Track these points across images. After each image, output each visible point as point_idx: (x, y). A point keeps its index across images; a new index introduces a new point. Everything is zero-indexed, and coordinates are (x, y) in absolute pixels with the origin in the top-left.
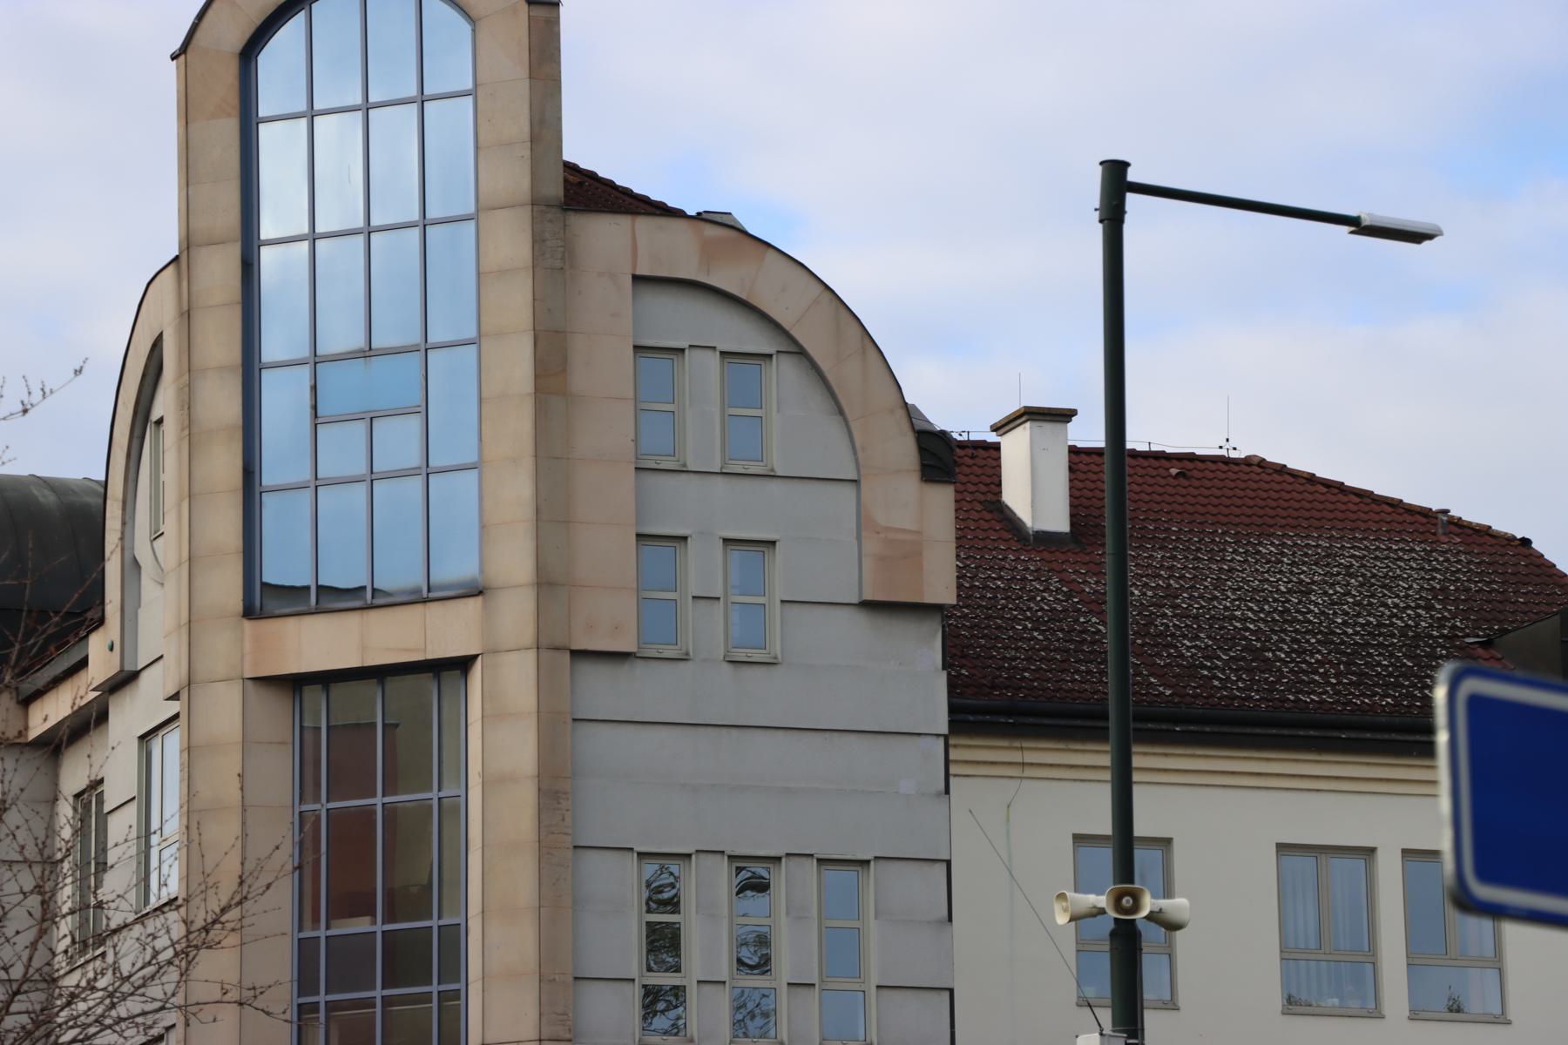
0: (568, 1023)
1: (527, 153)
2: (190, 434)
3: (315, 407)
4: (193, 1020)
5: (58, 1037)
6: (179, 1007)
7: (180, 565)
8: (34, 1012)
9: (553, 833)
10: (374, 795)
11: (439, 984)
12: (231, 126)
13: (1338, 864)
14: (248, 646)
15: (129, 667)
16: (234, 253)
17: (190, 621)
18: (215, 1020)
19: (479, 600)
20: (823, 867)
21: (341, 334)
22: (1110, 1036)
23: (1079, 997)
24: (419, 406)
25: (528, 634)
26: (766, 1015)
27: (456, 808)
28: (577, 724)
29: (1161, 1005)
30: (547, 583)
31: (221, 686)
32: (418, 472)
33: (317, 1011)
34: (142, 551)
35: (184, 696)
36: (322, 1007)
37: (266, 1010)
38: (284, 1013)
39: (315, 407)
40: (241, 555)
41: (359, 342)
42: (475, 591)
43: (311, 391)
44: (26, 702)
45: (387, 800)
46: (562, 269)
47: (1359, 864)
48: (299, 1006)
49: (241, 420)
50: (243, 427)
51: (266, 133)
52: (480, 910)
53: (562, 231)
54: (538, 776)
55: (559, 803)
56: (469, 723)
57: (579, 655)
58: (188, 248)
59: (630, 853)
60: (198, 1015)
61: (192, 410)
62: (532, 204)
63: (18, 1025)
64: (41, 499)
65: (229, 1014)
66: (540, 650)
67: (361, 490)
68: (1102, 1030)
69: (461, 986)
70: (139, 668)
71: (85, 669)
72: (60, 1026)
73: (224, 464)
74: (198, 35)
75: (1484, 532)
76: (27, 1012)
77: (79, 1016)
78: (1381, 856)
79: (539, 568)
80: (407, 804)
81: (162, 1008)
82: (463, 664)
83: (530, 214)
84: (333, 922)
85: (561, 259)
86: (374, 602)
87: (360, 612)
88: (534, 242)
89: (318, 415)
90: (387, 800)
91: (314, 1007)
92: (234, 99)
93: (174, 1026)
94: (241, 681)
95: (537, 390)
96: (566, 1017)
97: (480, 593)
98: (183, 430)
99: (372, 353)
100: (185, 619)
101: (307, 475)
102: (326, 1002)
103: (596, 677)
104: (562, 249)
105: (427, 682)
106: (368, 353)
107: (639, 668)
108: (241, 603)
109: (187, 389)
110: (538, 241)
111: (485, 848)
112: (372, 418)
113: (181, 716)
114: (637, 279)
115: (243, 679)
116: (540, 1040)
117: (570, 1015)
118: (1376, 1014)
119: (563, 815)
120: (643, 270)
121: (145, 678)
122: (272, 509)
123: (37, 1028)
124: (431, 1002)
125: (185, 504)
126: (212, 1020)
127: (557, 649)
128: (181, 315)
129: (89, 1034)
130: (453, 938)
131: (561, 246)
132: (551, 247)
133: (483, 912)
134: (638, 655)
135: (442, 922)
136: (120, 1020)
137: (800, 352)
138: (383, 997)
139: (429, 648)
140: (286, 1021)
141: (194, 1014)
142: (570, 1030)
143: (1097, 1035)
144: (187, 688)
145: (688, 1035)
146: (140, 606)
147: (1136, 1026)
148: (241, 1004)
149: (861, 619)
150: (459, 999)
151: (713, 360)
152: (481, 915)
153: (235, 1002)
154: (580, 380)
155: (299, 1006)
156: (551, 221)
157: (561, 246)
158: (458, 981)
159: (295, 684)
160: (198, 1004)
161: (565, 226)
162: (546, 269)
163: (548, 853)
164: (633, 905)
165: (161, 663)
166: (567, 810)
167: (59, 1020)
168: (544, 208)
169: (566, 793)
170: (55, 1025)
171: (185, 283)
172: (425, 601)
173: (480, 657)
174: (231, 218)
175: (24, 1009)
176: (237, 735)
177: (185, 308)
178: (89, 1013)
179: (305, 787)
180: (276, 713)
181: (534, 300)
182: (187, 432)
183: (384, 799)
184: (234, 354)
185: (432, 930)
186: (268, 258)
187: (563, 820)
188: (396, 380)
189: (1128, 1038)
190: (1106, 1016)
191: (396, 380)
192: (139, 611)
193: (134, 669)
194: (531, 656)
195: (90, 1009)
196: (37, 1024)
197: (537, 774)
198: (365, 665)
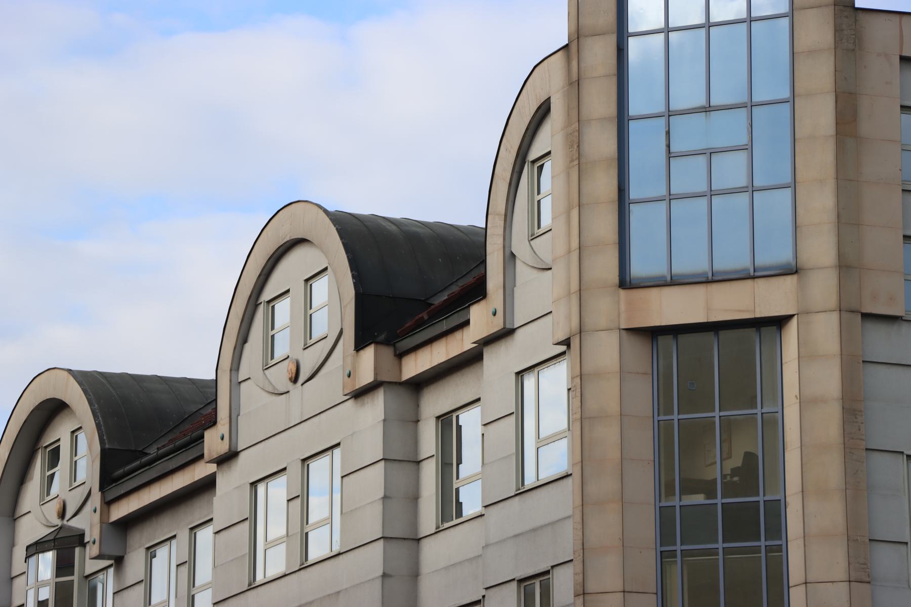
2: (579, 163)
3: (668, 146)
9: (853, 438)
14: (623, 307)
15: (508, 326)
16: (611, 41)
17: (580, 290)
19: (795, 277)
24: (747, 145)
25: (832, 300)
27: (775, 422)
31: (603, 334)
32: (746, 190)
33: (675, 556)
34: (520, 245)
35: (575, 343)
36: (679, 553)
39: (668, 146)
40: (618, 245)
41: (701, 101)
42: (792, 270)
43: (666, 135)
45: (722, 414)
46: (854, 50)
49: (617, 154)
50: (618, 159)
52: (801, 489)
53: (854, 24)
54: (842, 399)
55: (856, 418)
57: (866, 316)
58: (578, 38)
59: (901, 456)
61: (581, 147)
62: (835, 5)
64: (387, 227)
66: (841, 312)
67: (704, 202)
69: (783, 542)
70: (516, 326)
71: (468, 327)
79: (840, 255)
80: (738, 417)
82: (780, 322)
83: (833, 11)
84: (683, 497)
85: (853, 44)
86: (713, 278)
87: (705, 285)
88: (836, 30)
89: (671, 152)
90: (722, 414)
91: (673, 554)
94: (619, 330)
95: (837, 133)
96: (865, 566)
97: (796, 272)
98: (572, 161)
99: (711, 109)
100: (575, 286)
103: (877, 332)
104: (853, 36)
105: (751, 332)
106: (707, 109)
108: (618, 278)
109: (577, 134)
111: (803, 447)
112: (711, 153)
115: (620, 329)
116: (850, 581)
117: (869, 565)
119: (859, 426)
125: (575, 213)
127: (853, 312)
128: (571, 84)
130: (776, 510)
131: (853, 35)
132: (847, 35)
133: (803, 491)
134: (903, 318)
135: (766, 498)
139: (757, 309)
144: (578, 336)
146: (515, 286)
150: (781, 551)
152: (801, 493)
154: (866, 127)
156: (846, 17)
157: (853, 35)
161: (856, 20)
162: (843, 50)
163: (850, 452)
164: (904, 491)
165: (550, 316)
166: (862, 423)
168: (842, 8)
169: (861, 411)
171: (574, 63)
172: (754, 278)
173: (795, 319)
176: (616, 367)
177: (575, 77)
179: (662, 403)
181: (836, 71)
182: (576, 162)
183: (679, 416)
184: (611, 109)
185: (675, 508)
186: (634, 46)
187: (860, 430)
192: (515, 289)
193: (512, 327)
194: (835, 316)
197: (841, 397)
198: (710, 320)
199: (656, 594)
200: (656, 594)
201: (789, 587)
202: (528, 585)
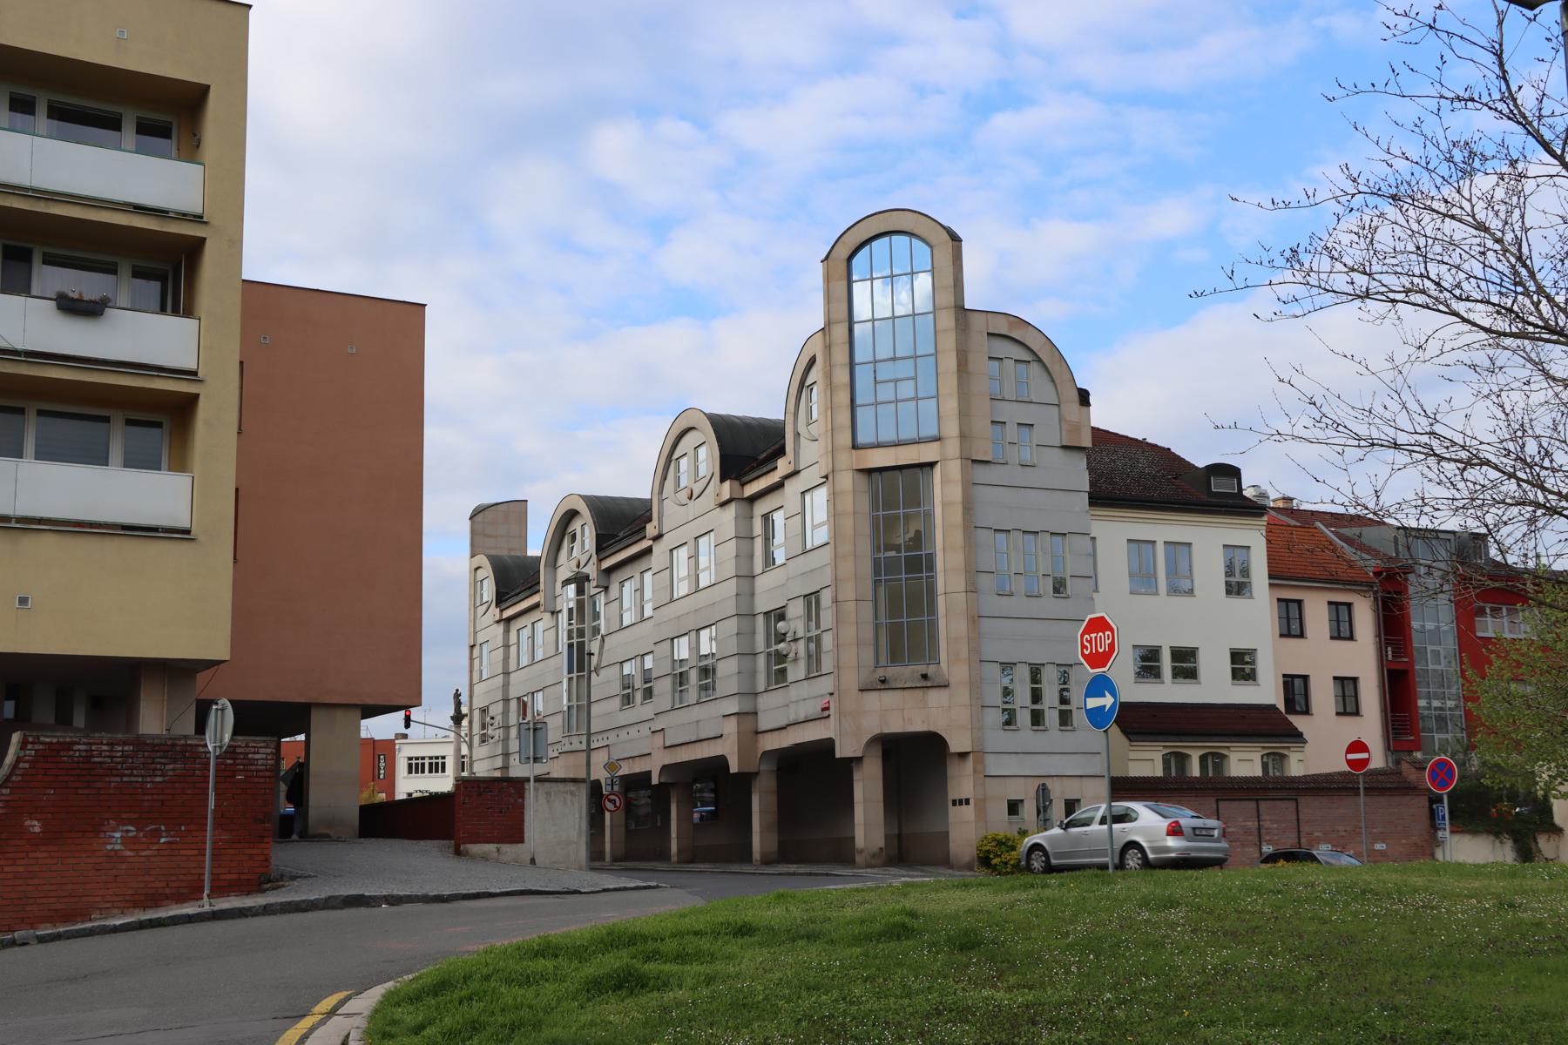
1: (953, 290)
7: (827, 431)
12: (844, 283)
13: (1144, 546)
15: (797, 469)
16: (847, 324)
19: (938, 443)
21: (884, 352)
25: (958, 454)
30: (964, 437)
42: (938, 439)
44: (743, 485)
47: (1150, 546)
51: (855, 286)
57: (974, 461)
73: (843, 397)
74: (832, 253)
75: (1156, 446)
78: (1158, 543)
82: (932, 465)
92: (845, 274)
95: (958, 370)
97: (939, 440)
100: (830, 449)
101: (874, 401)
103: (980, 469)
105: (917, 470)
106: (894, 359)
107: (992, 466)
110: (957, 320)
114: (989, 334)
118: (1157, 593)
120: (990, 331)
121: (802, 473)
122: (859, 411)
128: (826, 347)
130: (931, 558)
137: (1040, 361)
149: (1060, 452)
154: (972, 367)
159: (869, 471)
174: (844, 314)
179: (875, 505)
180: (863, 480)
184: (847, 360)
188: (905, 368)
191: (905, 368)
194: (959, 461)
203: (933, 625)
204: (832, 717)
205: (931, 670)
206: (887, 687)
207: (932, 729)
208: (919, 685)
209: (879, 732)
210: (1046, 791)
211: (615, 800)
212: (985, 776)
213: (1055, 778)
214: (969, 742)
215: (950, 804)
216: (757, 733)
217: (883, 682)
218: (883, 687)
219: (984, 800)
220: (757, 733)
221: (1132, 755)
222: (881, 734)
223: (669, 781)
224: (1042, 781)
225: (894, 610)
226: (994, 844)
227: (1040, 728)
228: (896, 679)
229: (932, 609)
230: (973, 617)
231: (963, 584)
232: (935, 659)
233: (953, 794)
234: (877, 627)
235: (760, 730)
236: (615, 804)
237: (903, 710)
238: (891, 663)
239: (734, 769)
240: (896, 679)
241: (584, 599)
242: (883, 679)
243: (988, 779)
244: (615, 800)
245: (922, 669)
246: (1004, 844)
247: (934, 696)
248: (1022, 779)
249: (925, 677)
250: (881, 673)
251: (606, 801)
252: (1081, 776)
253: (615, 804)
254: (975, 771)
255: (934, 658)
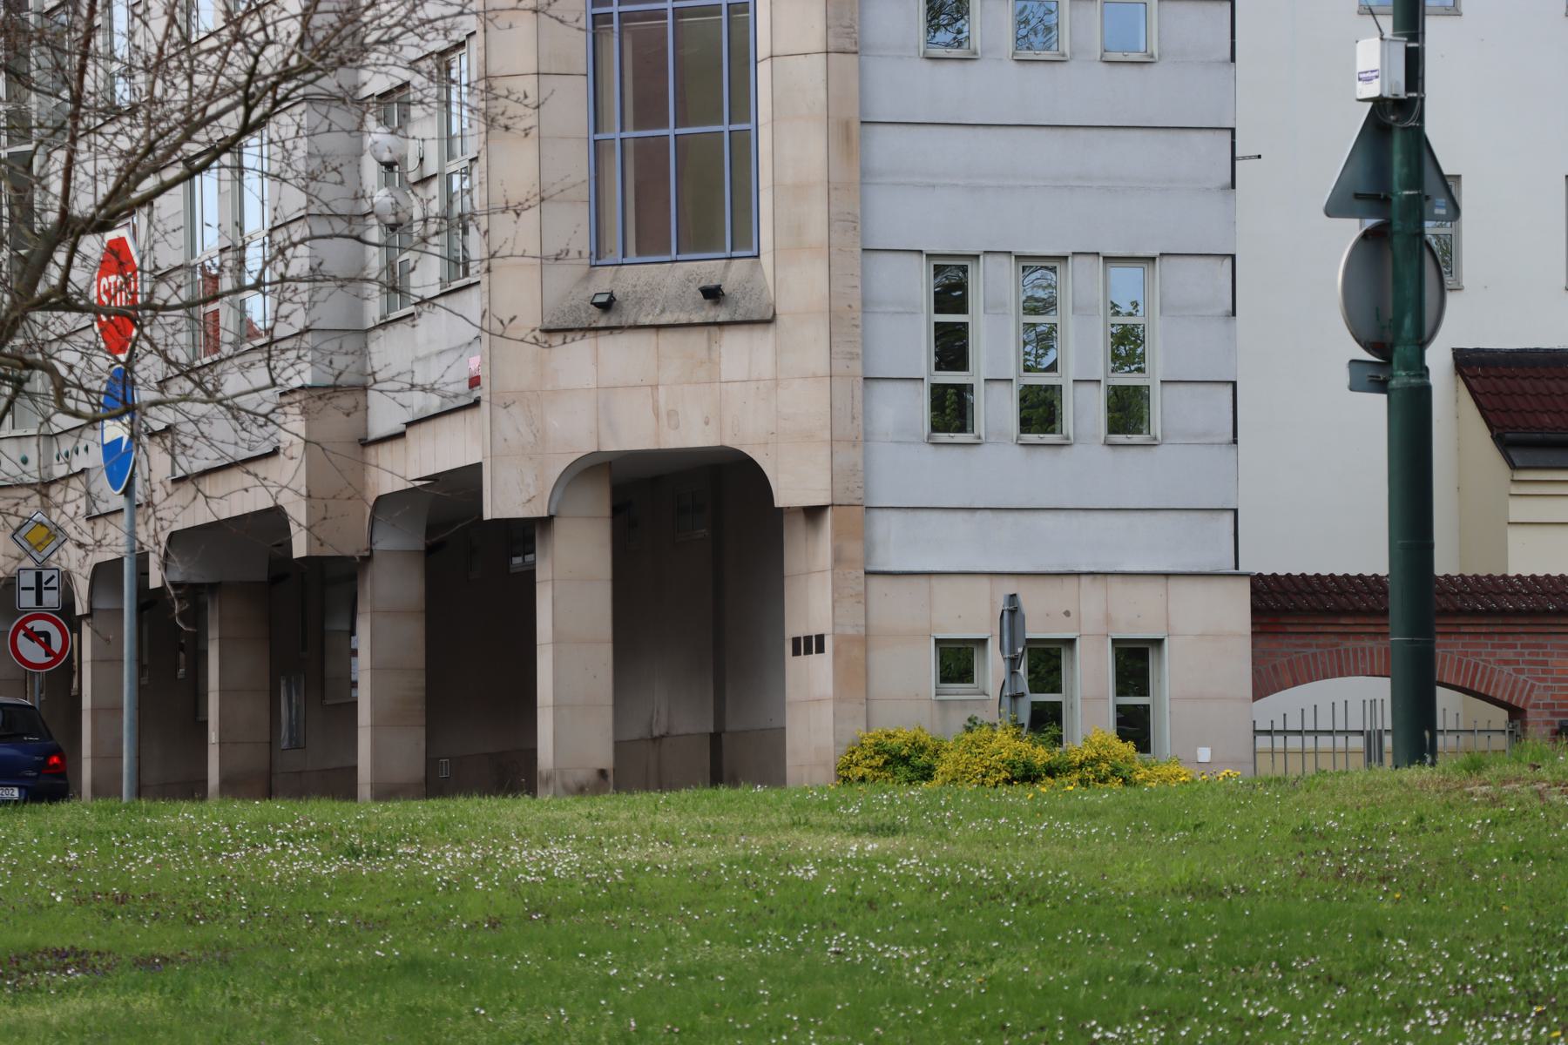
0: (854, 35)
4: (490, 27)
5: (364, 38)
6: (477, 13)
8: (341, 12)
10: (665, 125)
11: (730, 123)
18: (511, 27)
20: (1109, 265)
22: (1391, 40)
23: (1360, 6)
26: (1048, 30)
28: (869, 383)
29: (1444, 12)
33: (611, 21)
37: (560, 17)
38: (577, 21)
48: (594, 16)
56: (760, 188)
60: (495, 21)
63: (326, 23)
65: (526, 22)
68: (1382, 34)
69: (752, 126)
72: (365, 25)
76: (335, 12)
77: (383, 16)
81: (461, 13)
91: (608, 18)
93: (474, 33)
102: (619, 13)
113: (482, 403)
116: (827, 52)
117: (856, 27)
123: (345, 26)
124: (721, 14)
126: (507, 26)
129: (393, 35)
136: (423, 23)
138: (674, 9)
140: (579, 29)
141: (491, 20)
142: (856, 43)
143: (1378, 39)
145: (971, 47)
147: (1417, 29)
148: (536, 11)
150: (747, 11)
151: (1008, 268)
153: (530, 9)
155: (594, 16)
158: (749, 121)
160: (494, 10)
167: (365, 19)
170: (360, 24)
175: (331, 8)
178: (393, 13)
189: (1409, 41)
190: (1387, 23)
195: (393, 9)
196: (344, 23)
199: (586, 75)
200: (586, 75)
201: (756, 62)
202: (986, 428)
203: (744, 146)
204: (485, 405)
205: (731, 275)
206: (614, 322)
207: (729, 442)
208: (696, 319)
209: (595, 450)
210: (1018, 614)
211: (47, 635)
212: (868, 573)
213: (1085, 580)
214: (824, 480)
215: (789, 648)
216: (365, 443)
217: (606, 306)
218: (602, 324)
219: (865, 641)
220: (365, 443)
221: (1520, 510)
222: (598, 452)
223: (196, 580)
224: (1010, 587)
225: (647, 109)
226: (879, 761)
227: (1136, 438)
228: (639, 302)
229: (743, 104)
230: (847, 125)
231: (819, 26)
232: (750, 247)
233: (795, 627)
234: (598, 150)
235: (373, 436)
236: (47, 645)
237: (655, 387)
238: (639, 252)
239: (300, 547)
240: (639, 302)
241: (721, 20)
242: (604, 299)
243: (876, 582)
244: (47, 635)
245: (709, 270)
246: (905, 760)
247: (734, 343)
248: (985, 581)
249: (713, 294)
250: (604, 282)
251: (21, 638)
252: (1167, 575)
253: (47, 645)
254: (838, 559)
255: (744, 239)
